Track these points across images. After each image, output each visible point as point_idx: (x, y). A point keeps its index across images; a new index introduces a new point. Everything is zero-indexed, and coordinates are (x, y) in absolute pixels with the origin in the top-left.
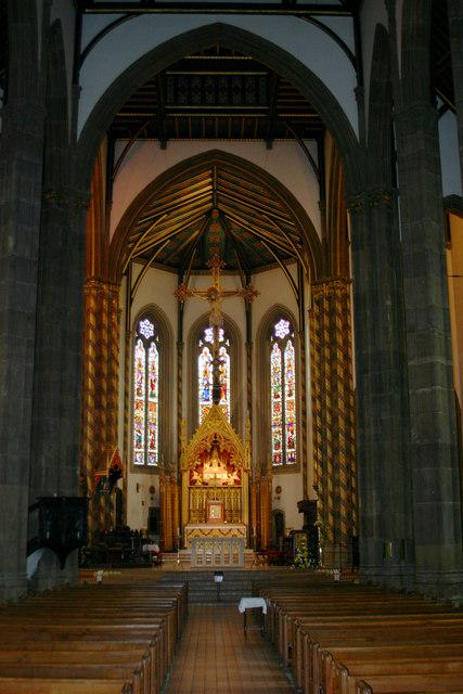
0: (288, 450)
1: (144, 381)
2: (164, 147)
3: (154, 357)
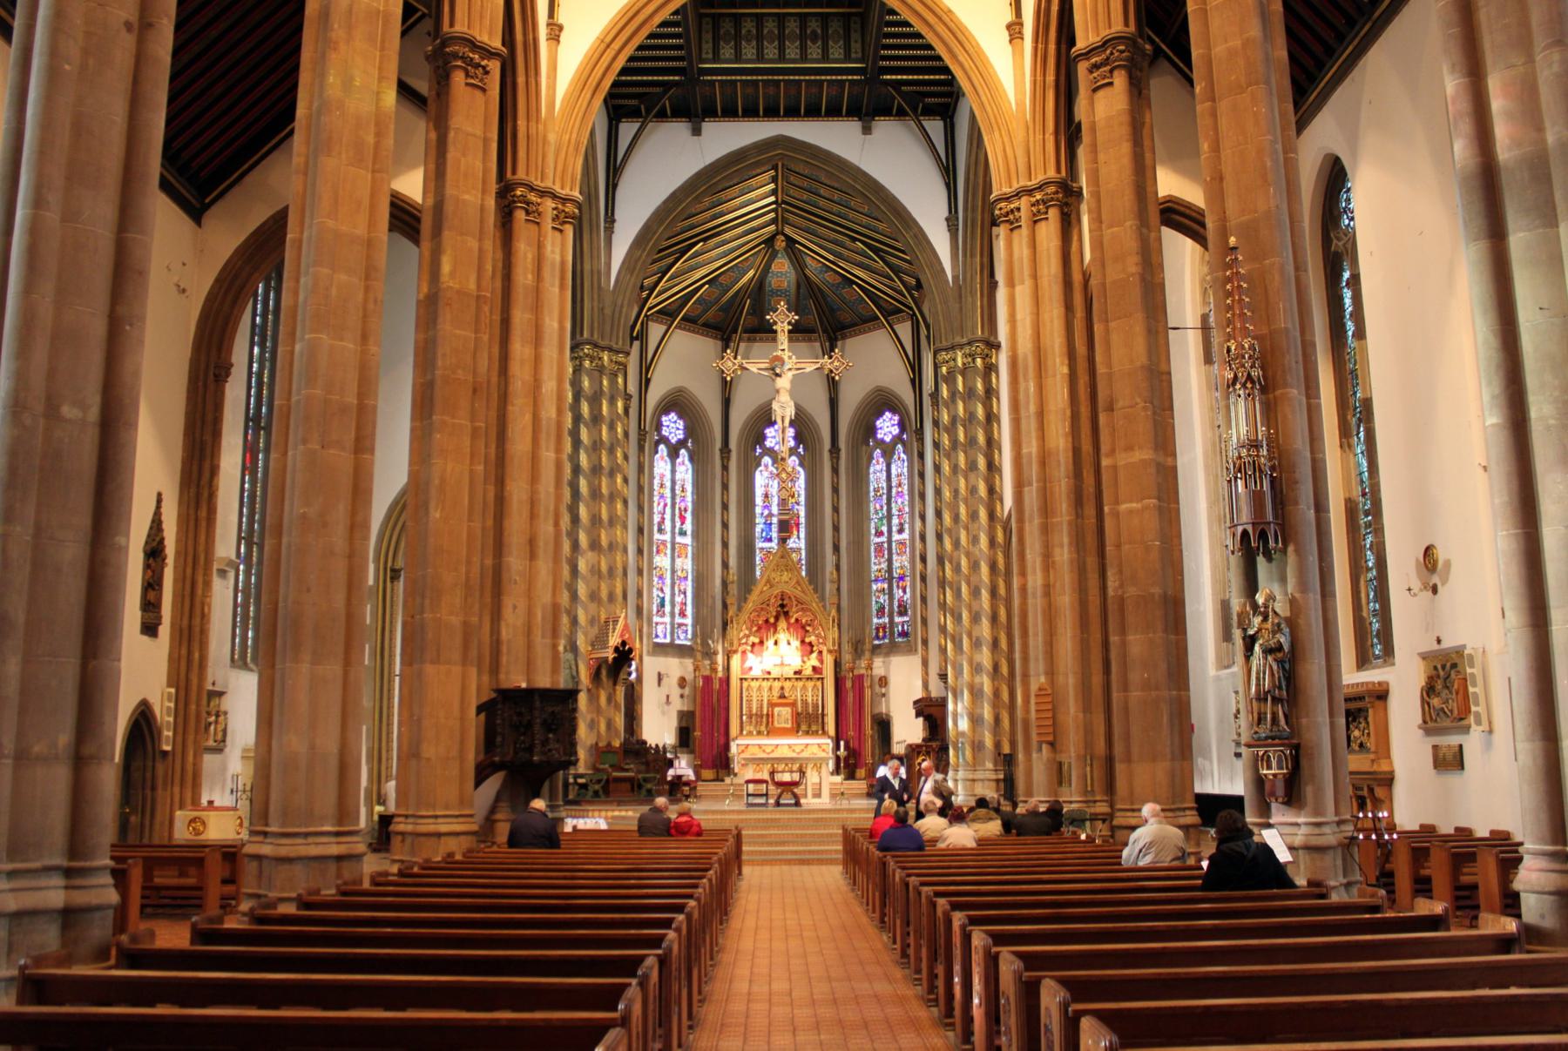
0: (897, 619)
1: (668, 510)
2: (697, 132)
3: (685, 471)
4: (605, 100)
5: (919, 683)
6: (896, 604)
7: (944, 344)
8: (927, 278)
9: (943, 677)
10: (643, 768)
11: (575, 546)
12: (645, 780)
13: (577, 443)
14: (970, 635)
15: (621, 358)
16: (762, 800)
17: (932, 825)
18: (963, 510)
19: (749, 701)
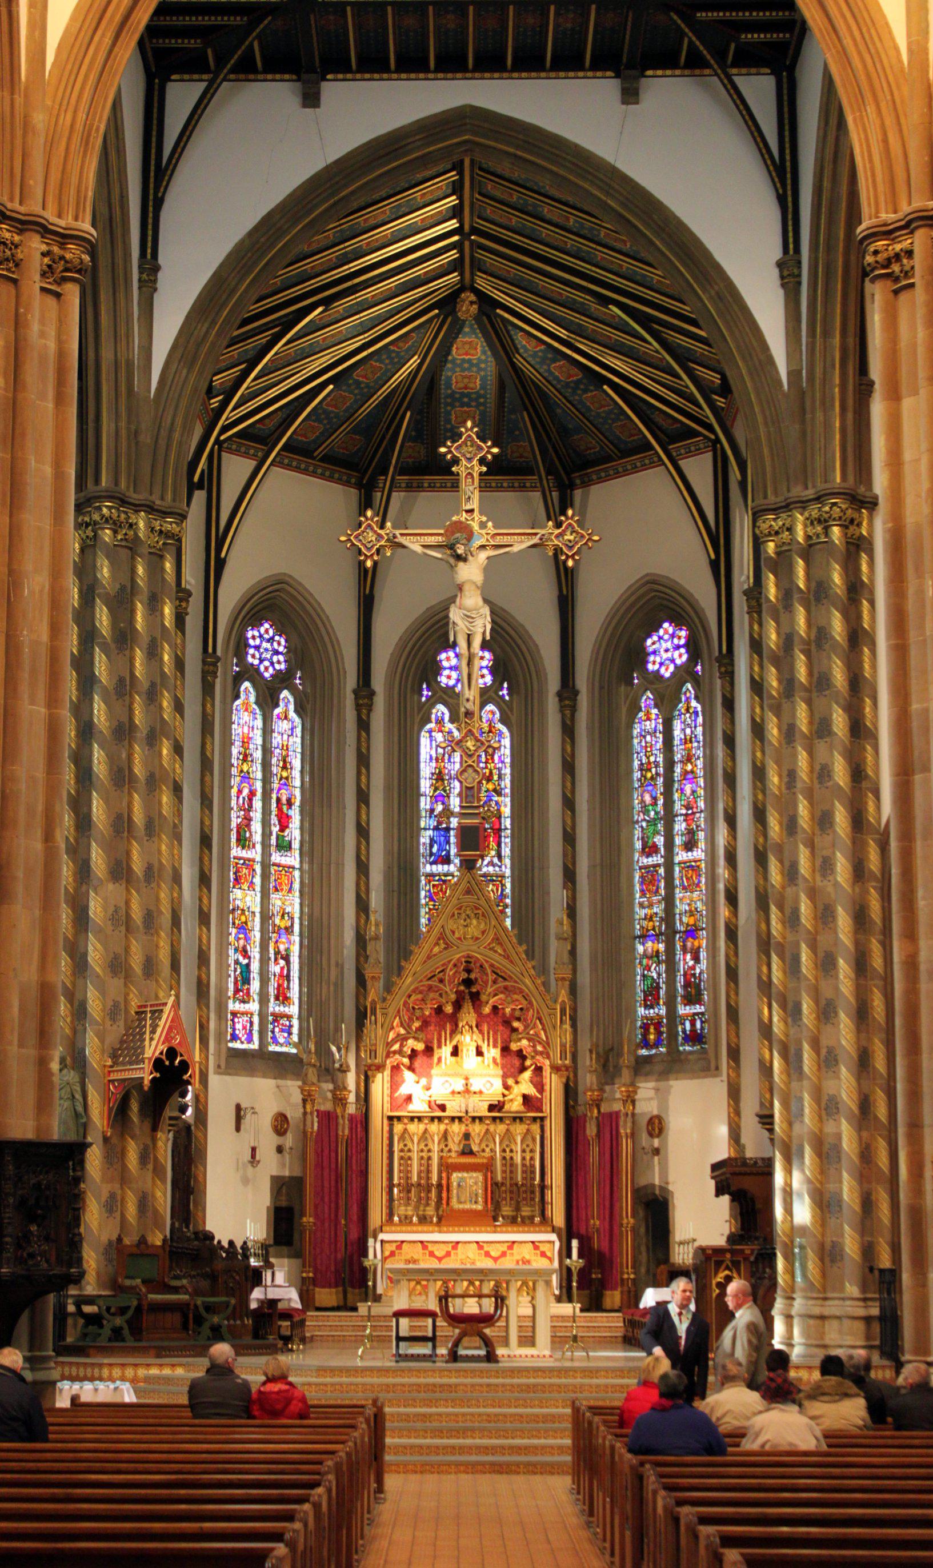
0: (683, 1010)
1: (258, 804)
2: (311, 99)
3: (289, 730)
4: (141, 43)
5: (723, 1130)
6: (680, 980)
7: (772, 499)
8: (741, 375)
9: (766, 1120)
10: (205, 1284)
11: (83, 872)
12: (209, 1308)
13: (87, 682)
14: (816, 1045)
15: (169, 524)
16: (425, 1349)
17: (730, 1403)
18: (803, 809)
19: (406, 1160)
